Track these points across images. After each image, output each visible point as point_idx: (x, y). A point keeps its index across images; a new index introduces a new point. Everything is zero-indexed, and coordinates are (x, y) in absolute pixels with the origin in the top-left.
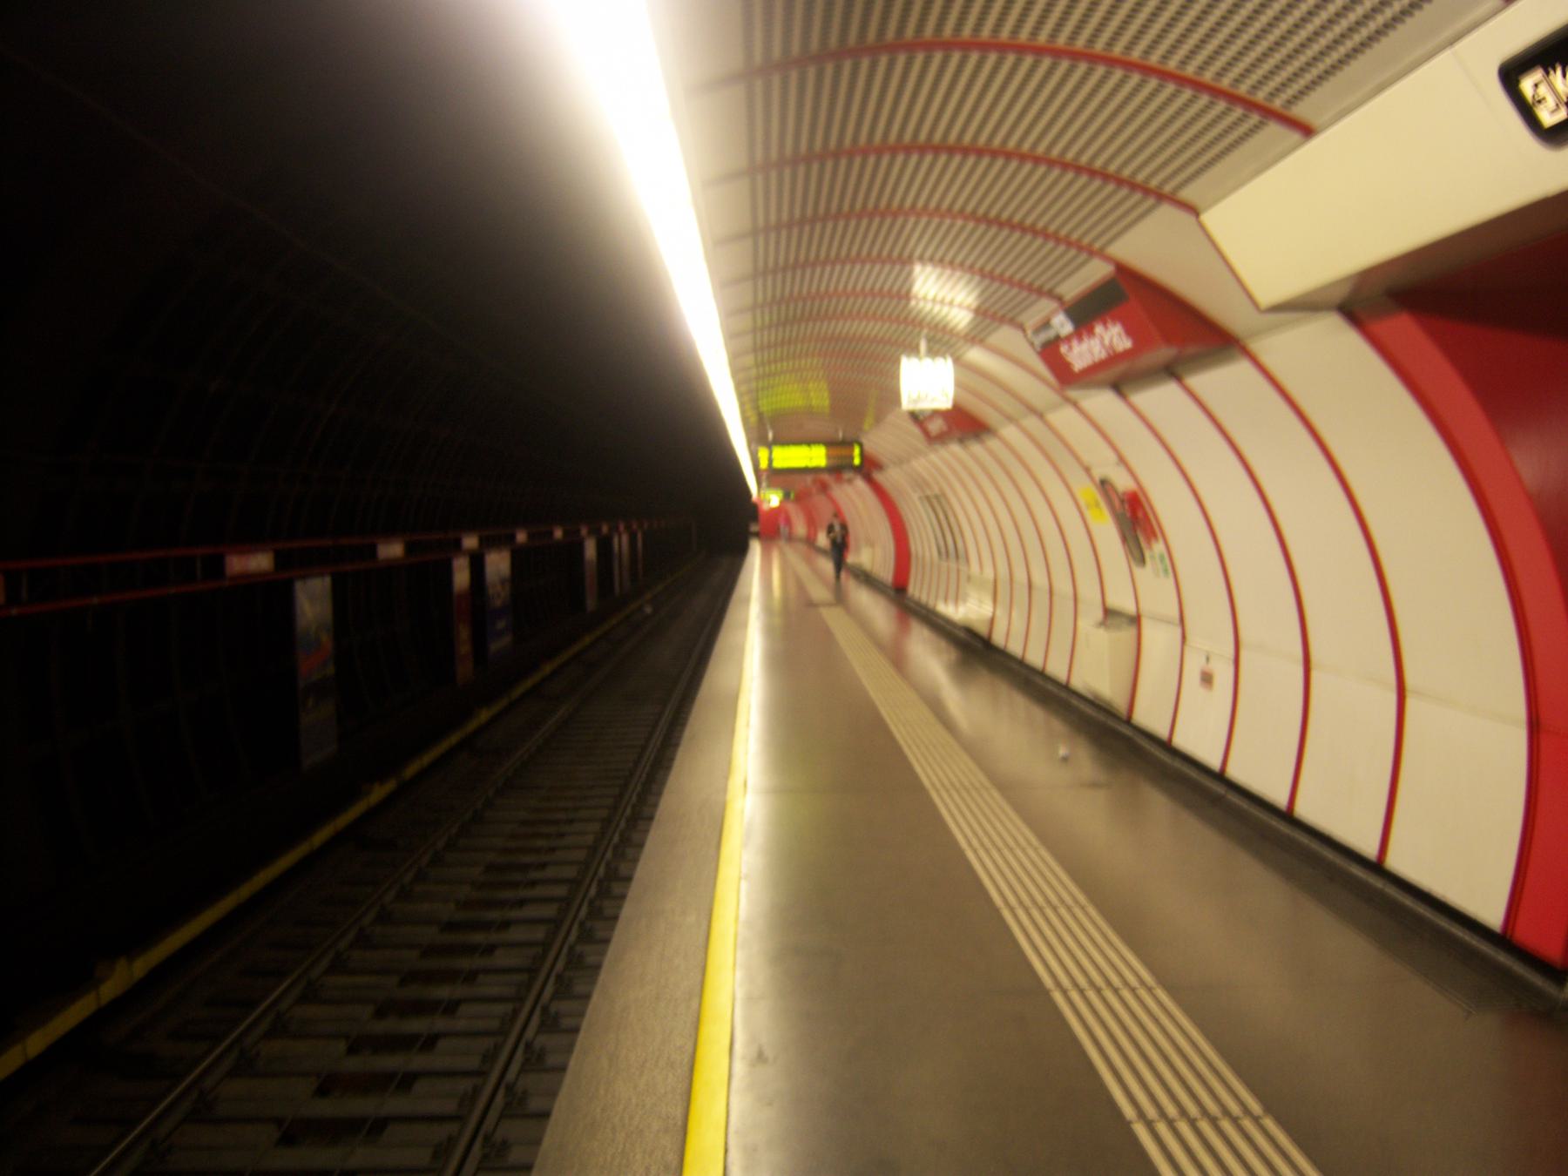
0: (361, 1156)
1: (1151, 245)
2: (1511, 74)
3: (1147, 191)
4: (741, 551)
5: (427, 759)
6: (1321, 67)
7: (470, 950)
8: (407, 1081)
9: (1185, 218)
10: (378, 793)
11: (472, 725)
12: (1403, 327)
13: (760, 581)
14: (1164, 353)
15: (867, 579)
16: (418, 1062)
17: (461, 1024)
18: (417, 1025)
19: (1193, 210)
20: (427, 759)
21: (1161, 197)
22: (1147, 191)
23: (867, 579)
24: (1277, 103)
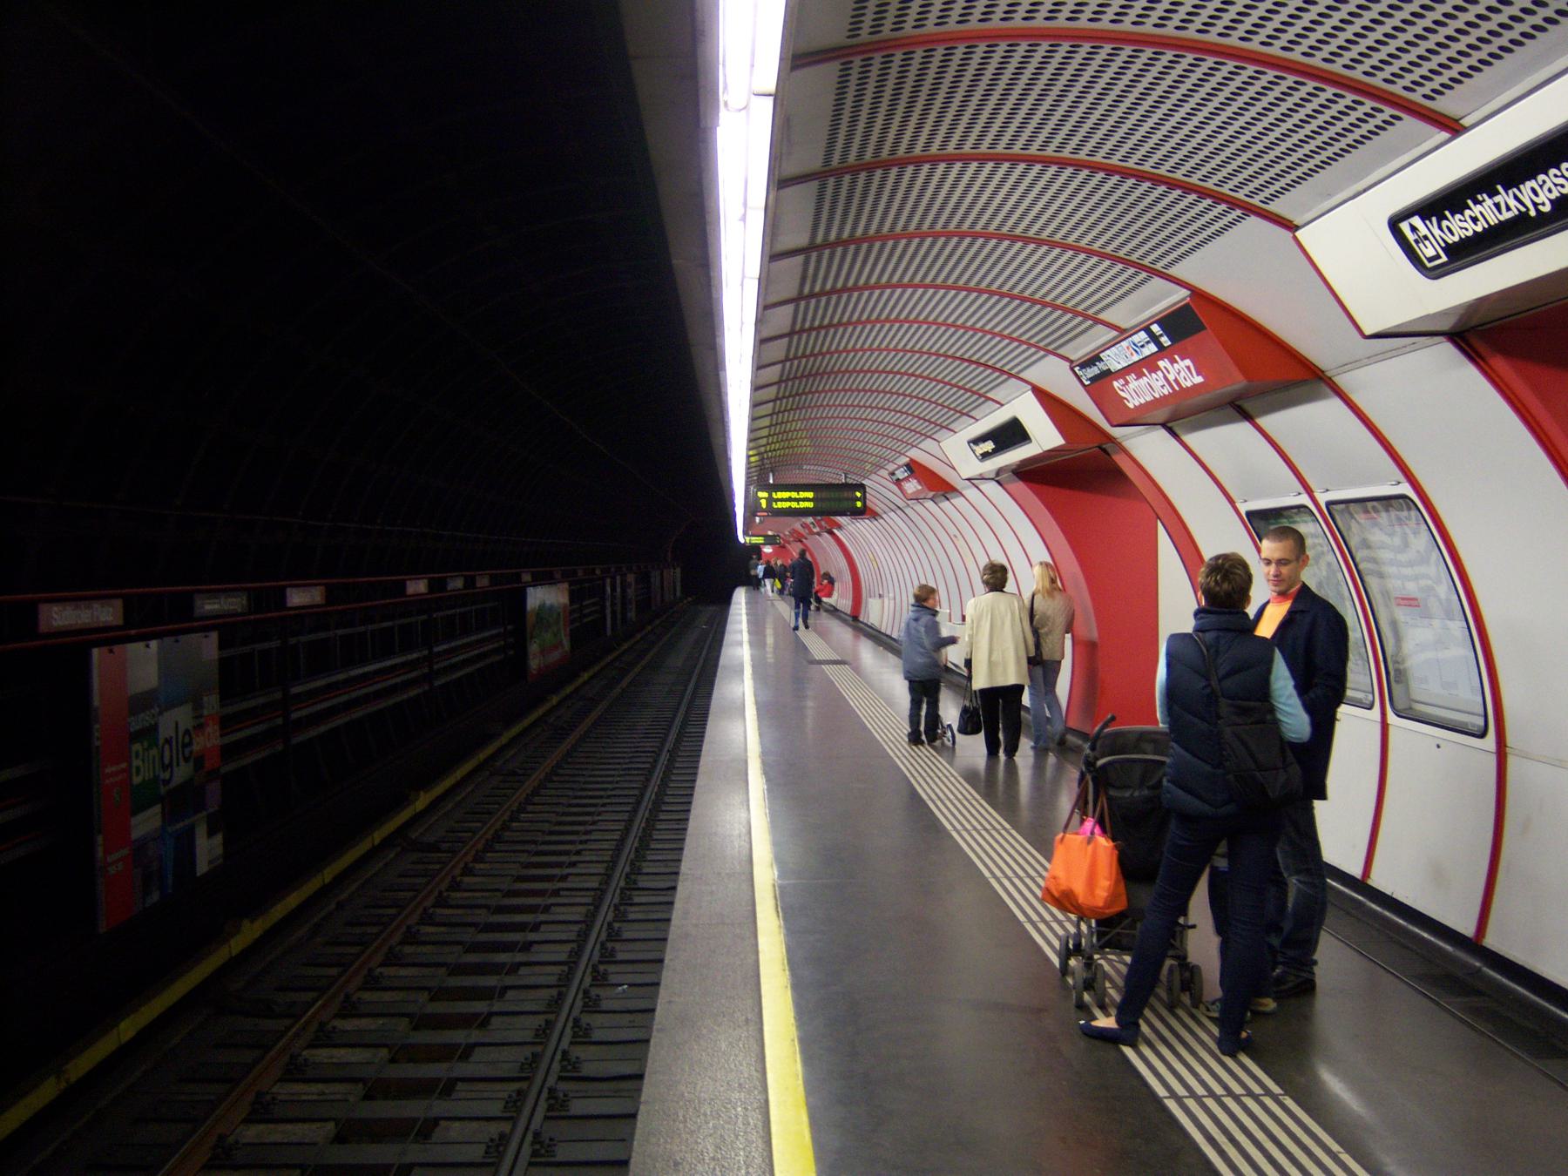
0: (414, 1152)
1: (922, 454)
2: (1394, 224)
3: (1003, 372)
4: (726, 600)
5: (293, 900)
6: (1288, 179)
7: (496, 969)
8: (527, 947)
9: (1289, 234)
10: (251, 931)
11: (580, 681)
12: (1020, 487)
13: (747, 631)
14: (931, 494)
15: (879, 638)
16: (532, 936)
17: (458, 1108)
18: (414, 1109)
19: (1291, 227)
20: (293, 900)
21: (1011, 376)
22: (1003, 372)
23: (879, 638)
24: (1158, 266)
